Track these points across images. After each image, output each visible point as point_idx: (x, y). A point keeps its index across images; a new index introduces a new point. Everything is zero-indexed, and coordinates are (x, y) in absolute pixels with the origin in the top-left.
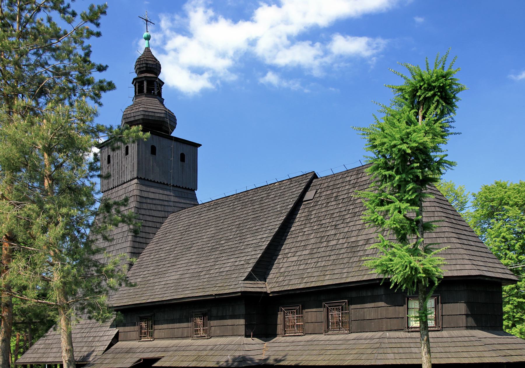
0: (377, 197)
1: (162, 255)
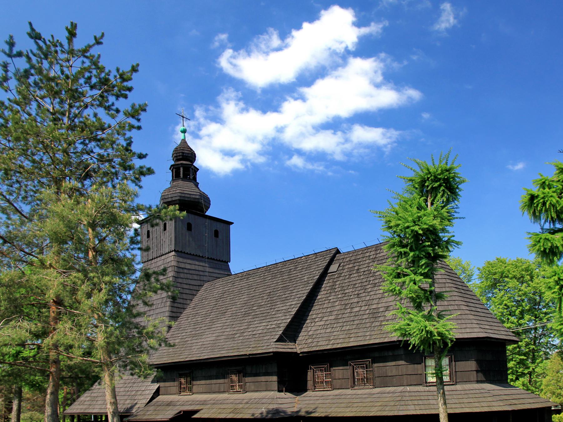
0: (394, 271)
1: (198, 319)
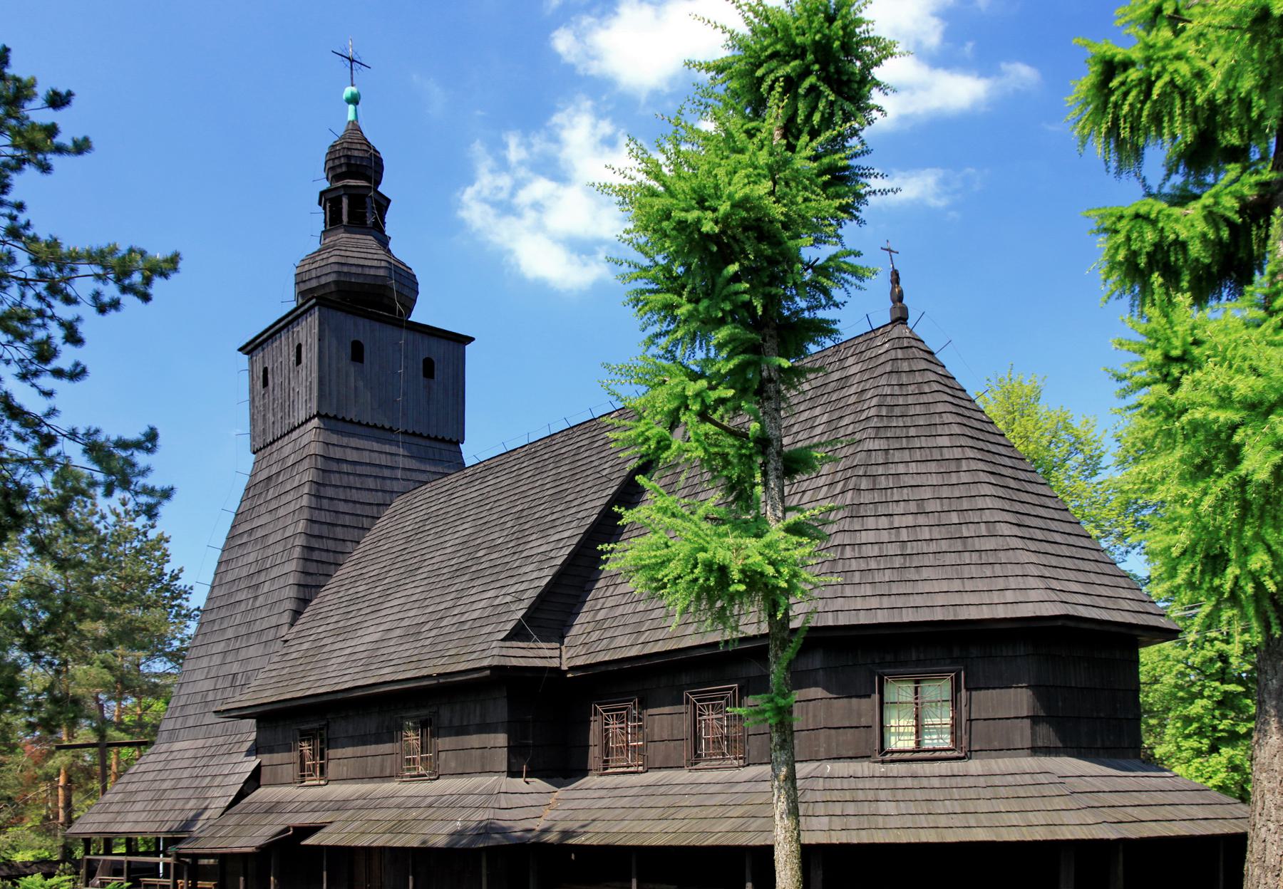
1: (360, 589)
